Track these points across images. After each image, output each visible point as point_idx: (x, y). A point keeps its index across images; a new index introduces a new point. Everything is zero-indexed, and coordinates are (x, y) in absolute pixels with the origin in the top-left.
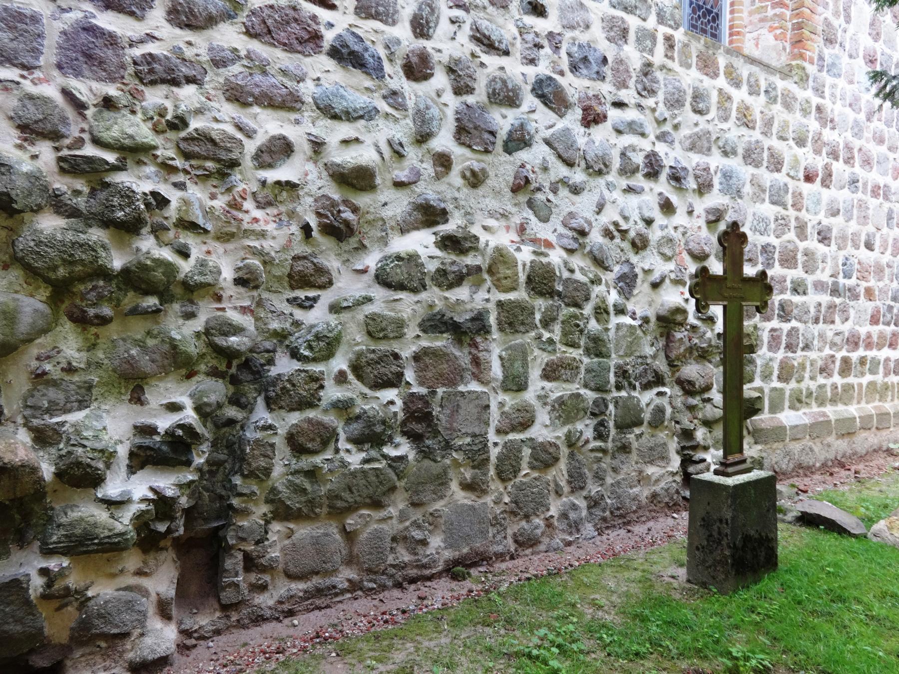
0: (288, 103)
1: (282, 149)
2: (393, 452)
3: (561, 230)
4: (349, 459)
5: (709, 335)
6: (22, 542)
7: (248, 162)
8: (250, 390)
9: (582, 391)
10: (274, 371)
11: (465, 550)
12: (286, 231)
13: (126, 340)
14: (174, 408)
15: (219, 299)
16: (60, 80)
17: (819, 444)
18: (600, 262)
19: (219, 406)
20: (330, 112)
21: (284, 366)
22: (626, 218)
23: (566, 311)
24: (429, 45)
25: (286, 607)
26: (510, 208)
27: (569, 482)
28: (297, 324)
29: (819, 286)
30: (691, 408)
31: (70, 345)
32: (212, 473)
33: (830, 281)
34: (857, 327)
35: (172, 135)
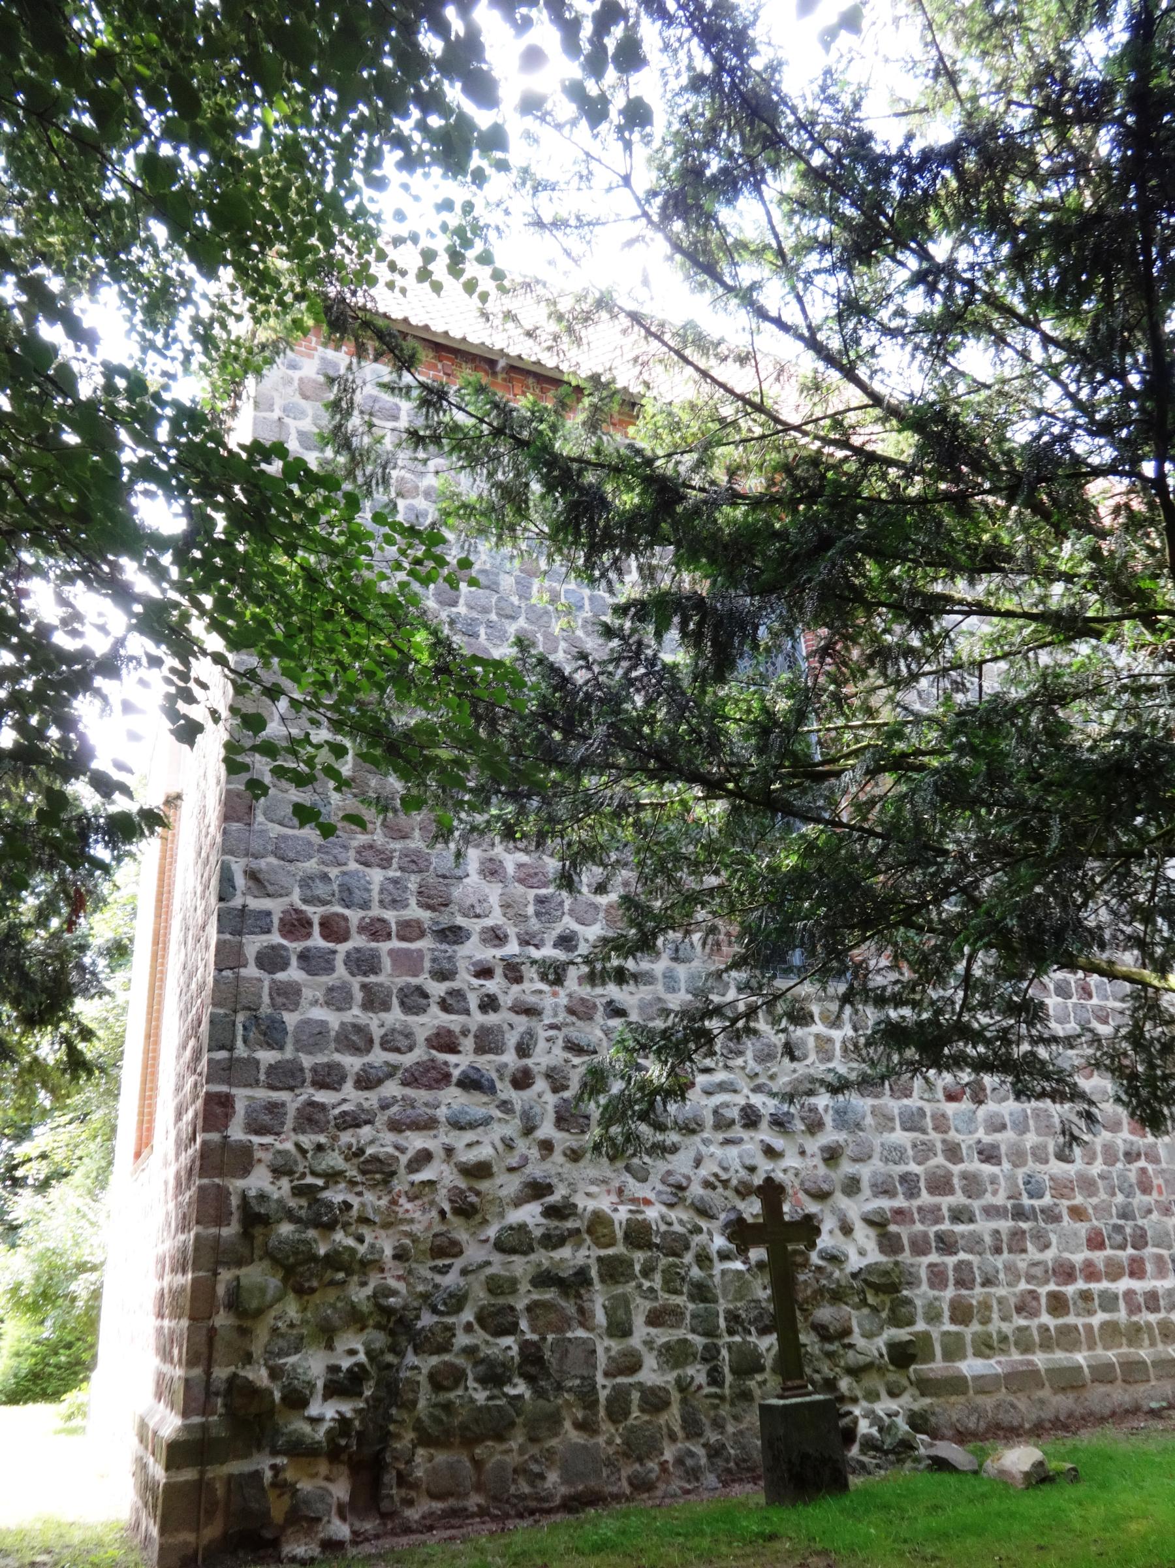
0: (428, 1125)
1: (424, 1158)
2: (512, 1392)
3: (660, 1187)
4: (476, 1396)
5: (837, 1274)
6: (259, 1448)
7: (402, 1170)
8: (403, 1340)
9: (690, 1337)
10: (420, 1325)
11: (581, 1488)
12: (428, 1216)
13: (325, 1301)
14: (352, 1352)
15: (382, 1270)
16: (294, 1137)
17: (1024, 1399)
18: (704, 1212)
19: (382, 1352)
20: (457, 1125)
21: (427, 1320)
22: (725, 1169)
23: (664, 1261)
24: (529, 1062)
25: (428, 1522)
26: (609, 1174)
27: (683, 1428)
28: (437, 1286)
29: (992, 1212)
30: (830, 1355)
31: (292, 1309)
32: (375, 1408)
33: (1009, 1204)
34: (1066, 1255)
35: (355, 1161)
